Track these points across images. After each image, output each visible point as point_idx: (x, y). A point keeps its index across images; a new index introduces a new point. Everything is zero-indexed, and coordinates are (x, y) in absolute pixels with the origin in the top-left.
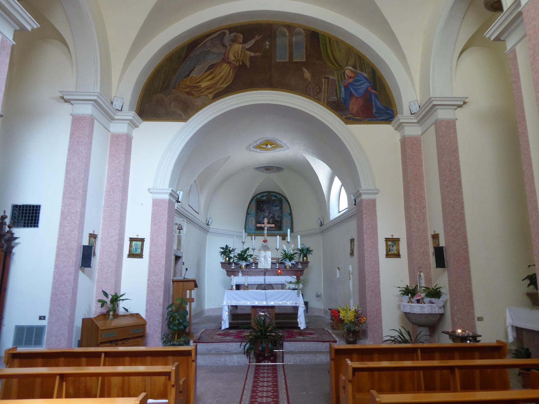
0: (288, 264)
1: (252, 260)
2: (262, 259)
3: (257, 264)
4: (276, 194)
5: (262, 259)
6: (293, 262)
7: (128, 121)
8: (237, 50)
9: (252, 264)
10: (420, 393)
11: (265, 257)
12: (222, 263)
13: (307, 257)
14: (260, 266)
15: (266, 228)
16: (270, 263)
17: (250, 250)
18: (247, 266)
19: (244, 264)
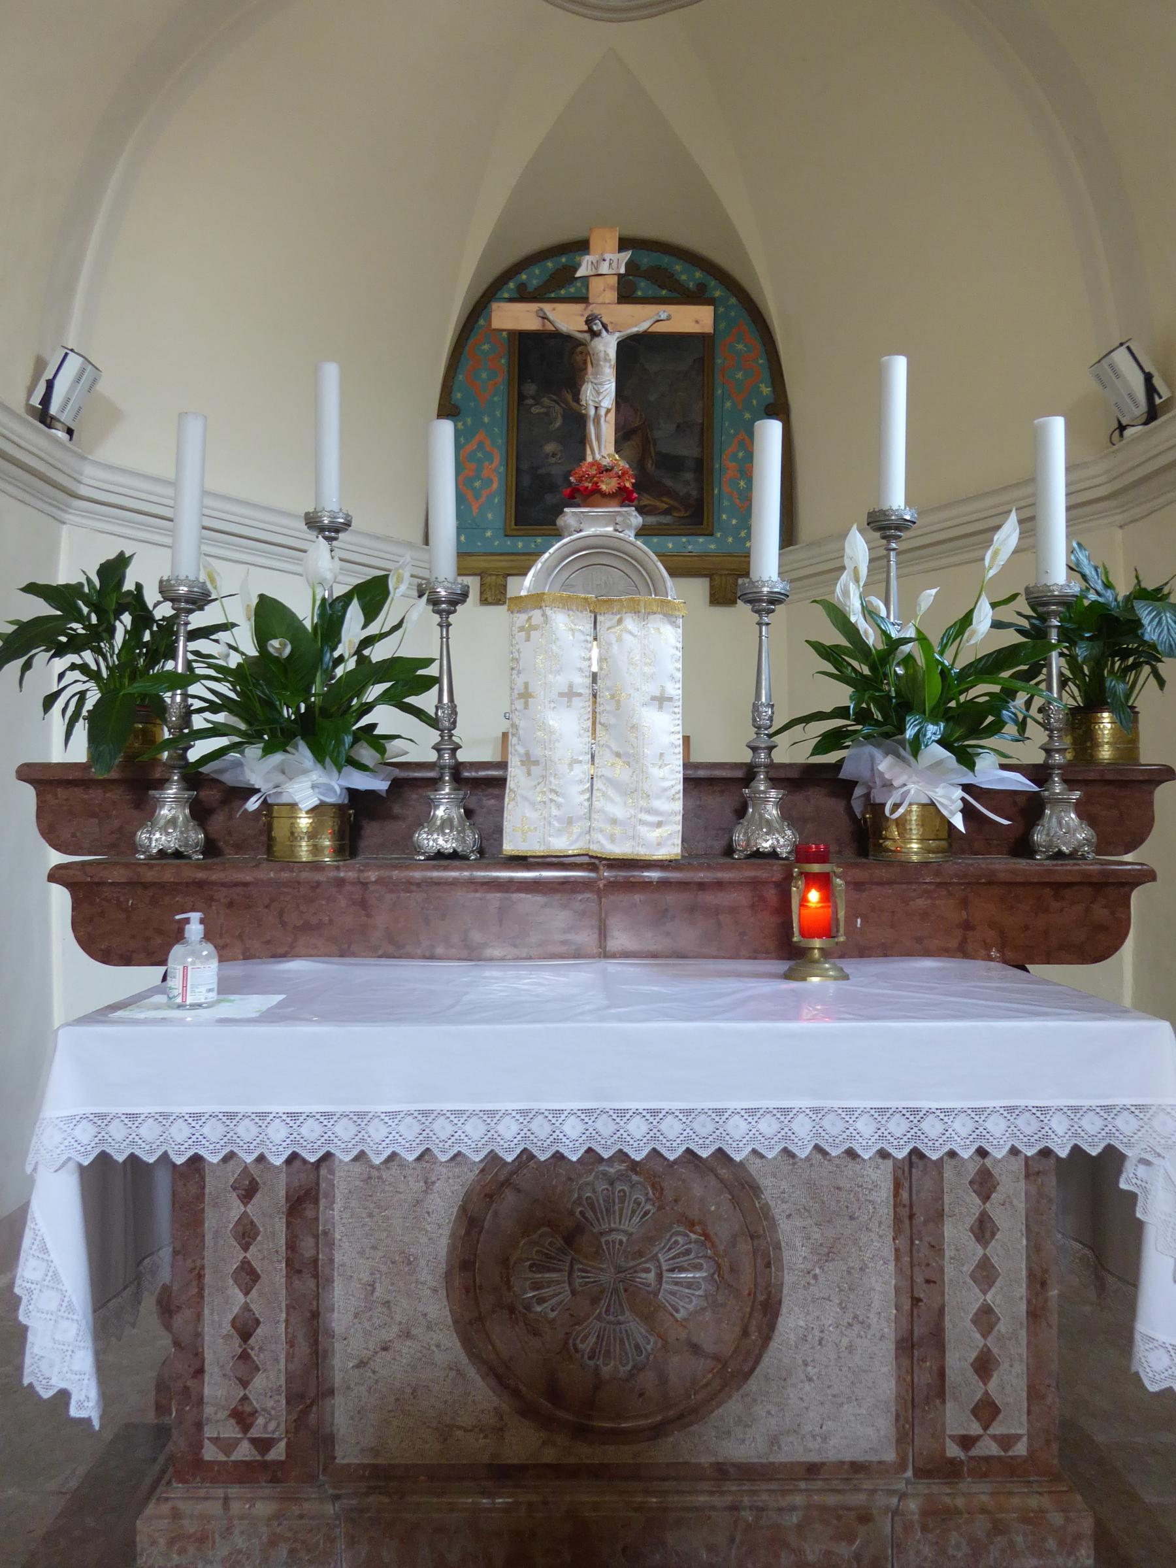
0: (924, 787)
1: (414, 742)
2: (565, 727)
3: (483, 786)
4: (665, 260)
5: (565, 727)
6: (990, 773)
7: (83, 491)
8: (462, 439)
9: (411, 785)
10: (509, 1141)
11: (599, 695)
12: (43, 779)
13: (1128, 717)
14: (527, 825)
15: (607, 347)
16: (669, 777)
17: (402, 601)
18: (355, 819)
19: (304, 787)
